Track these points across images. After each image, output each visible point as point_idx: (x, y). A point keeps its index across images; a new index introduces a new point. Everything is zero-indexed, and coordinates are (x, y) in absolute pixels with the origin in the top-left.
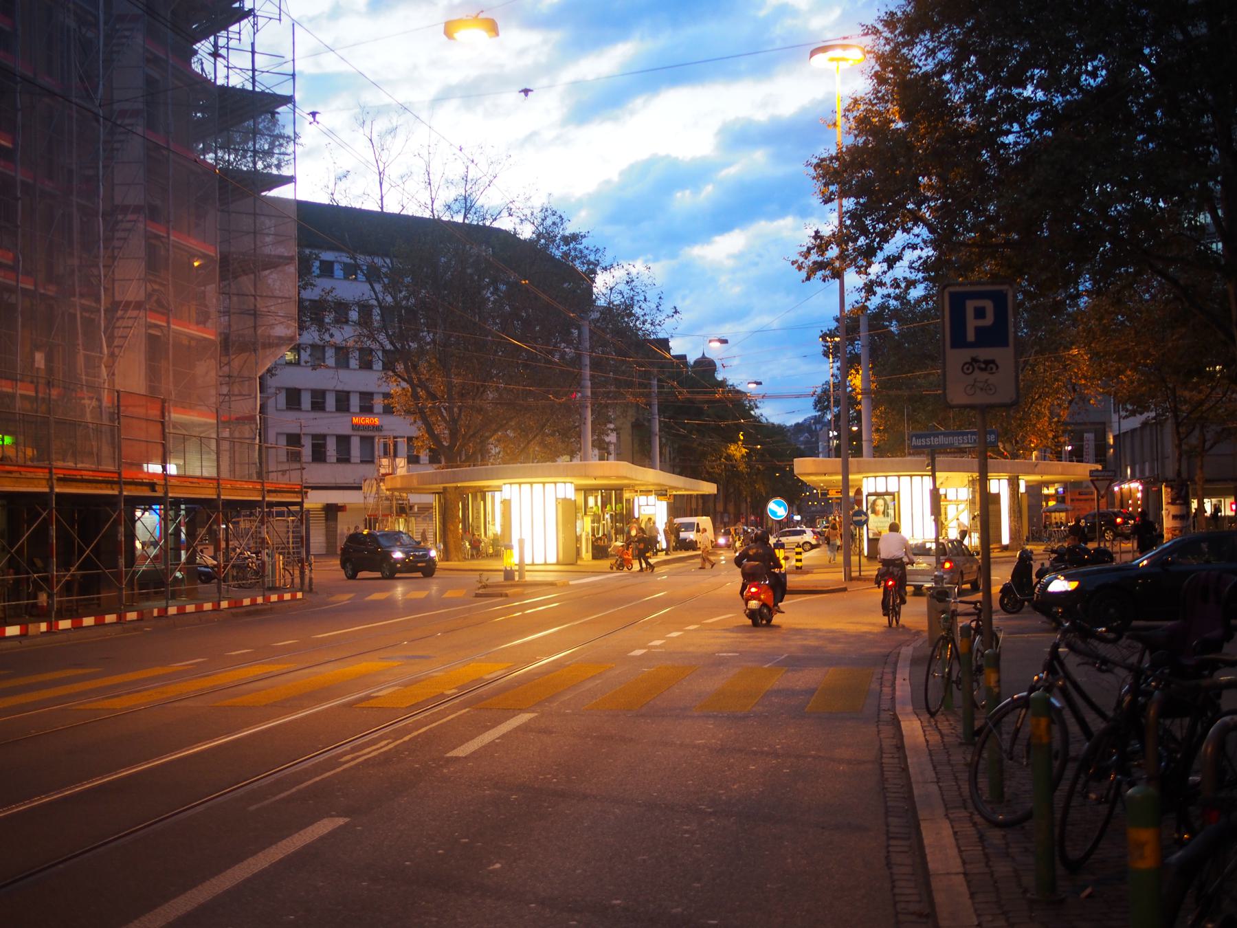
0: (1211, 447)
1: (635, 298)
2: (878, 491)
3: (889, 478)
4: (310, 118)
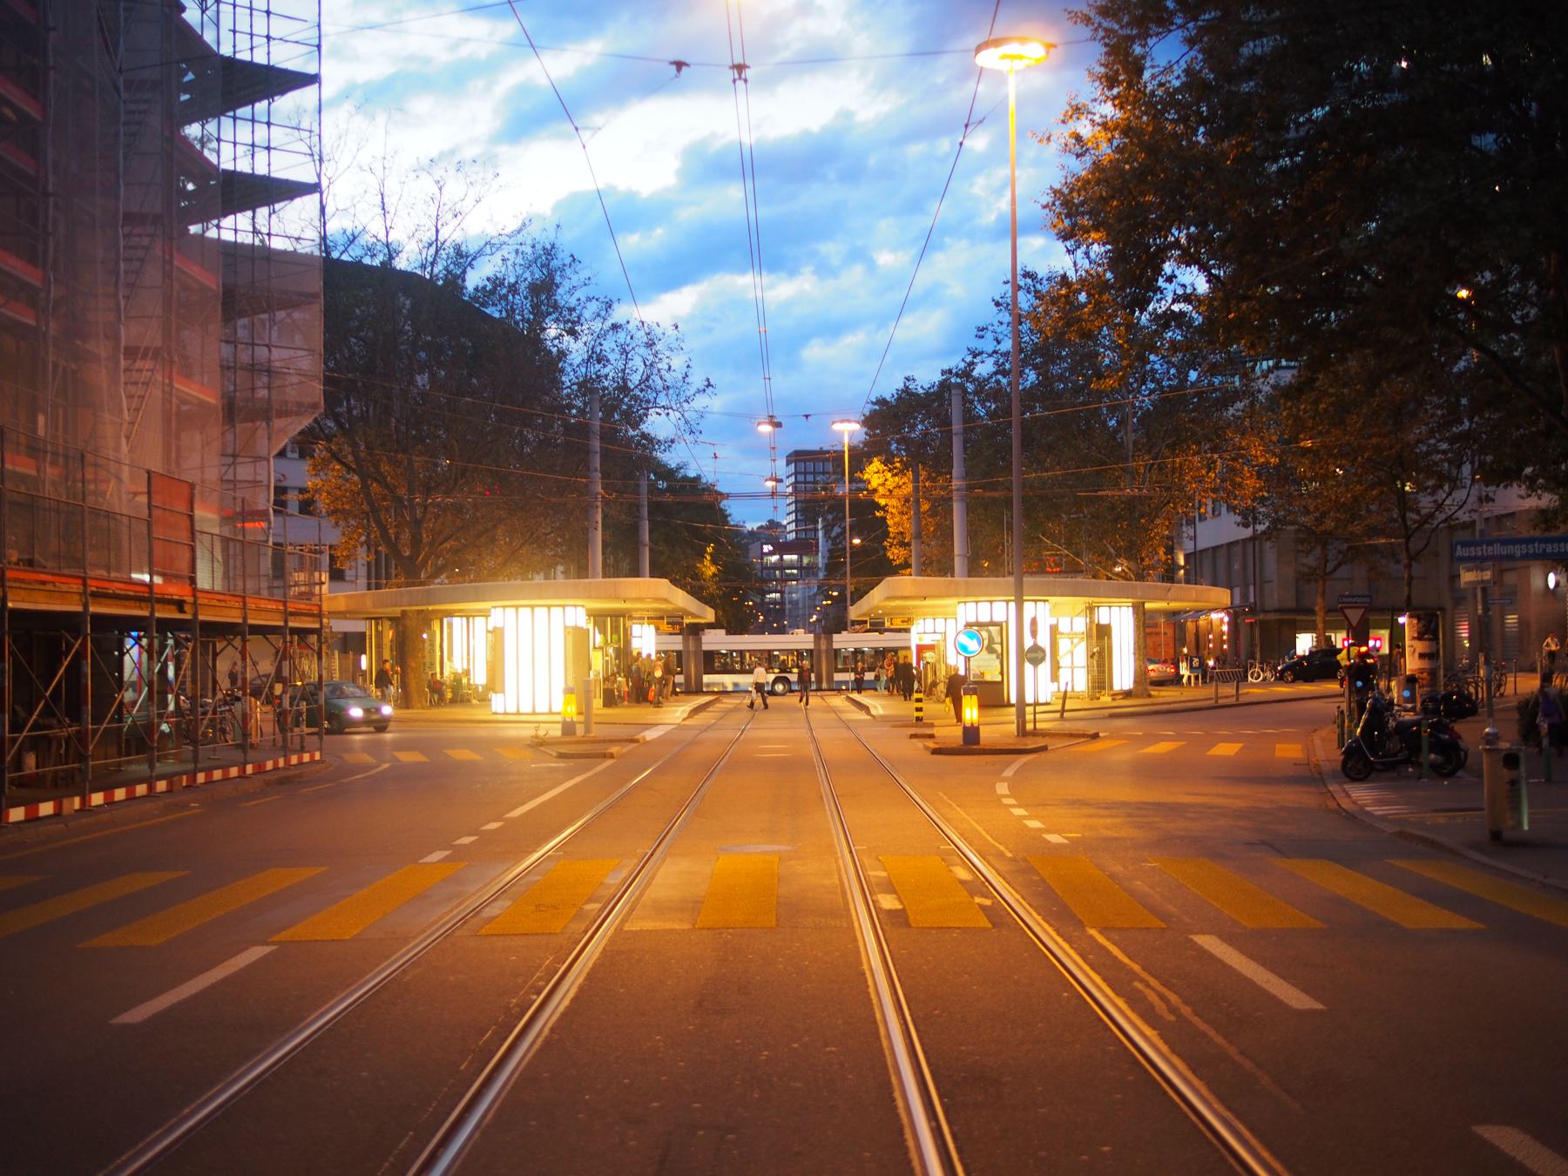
0: (1335, 569)
3: (994, 604)
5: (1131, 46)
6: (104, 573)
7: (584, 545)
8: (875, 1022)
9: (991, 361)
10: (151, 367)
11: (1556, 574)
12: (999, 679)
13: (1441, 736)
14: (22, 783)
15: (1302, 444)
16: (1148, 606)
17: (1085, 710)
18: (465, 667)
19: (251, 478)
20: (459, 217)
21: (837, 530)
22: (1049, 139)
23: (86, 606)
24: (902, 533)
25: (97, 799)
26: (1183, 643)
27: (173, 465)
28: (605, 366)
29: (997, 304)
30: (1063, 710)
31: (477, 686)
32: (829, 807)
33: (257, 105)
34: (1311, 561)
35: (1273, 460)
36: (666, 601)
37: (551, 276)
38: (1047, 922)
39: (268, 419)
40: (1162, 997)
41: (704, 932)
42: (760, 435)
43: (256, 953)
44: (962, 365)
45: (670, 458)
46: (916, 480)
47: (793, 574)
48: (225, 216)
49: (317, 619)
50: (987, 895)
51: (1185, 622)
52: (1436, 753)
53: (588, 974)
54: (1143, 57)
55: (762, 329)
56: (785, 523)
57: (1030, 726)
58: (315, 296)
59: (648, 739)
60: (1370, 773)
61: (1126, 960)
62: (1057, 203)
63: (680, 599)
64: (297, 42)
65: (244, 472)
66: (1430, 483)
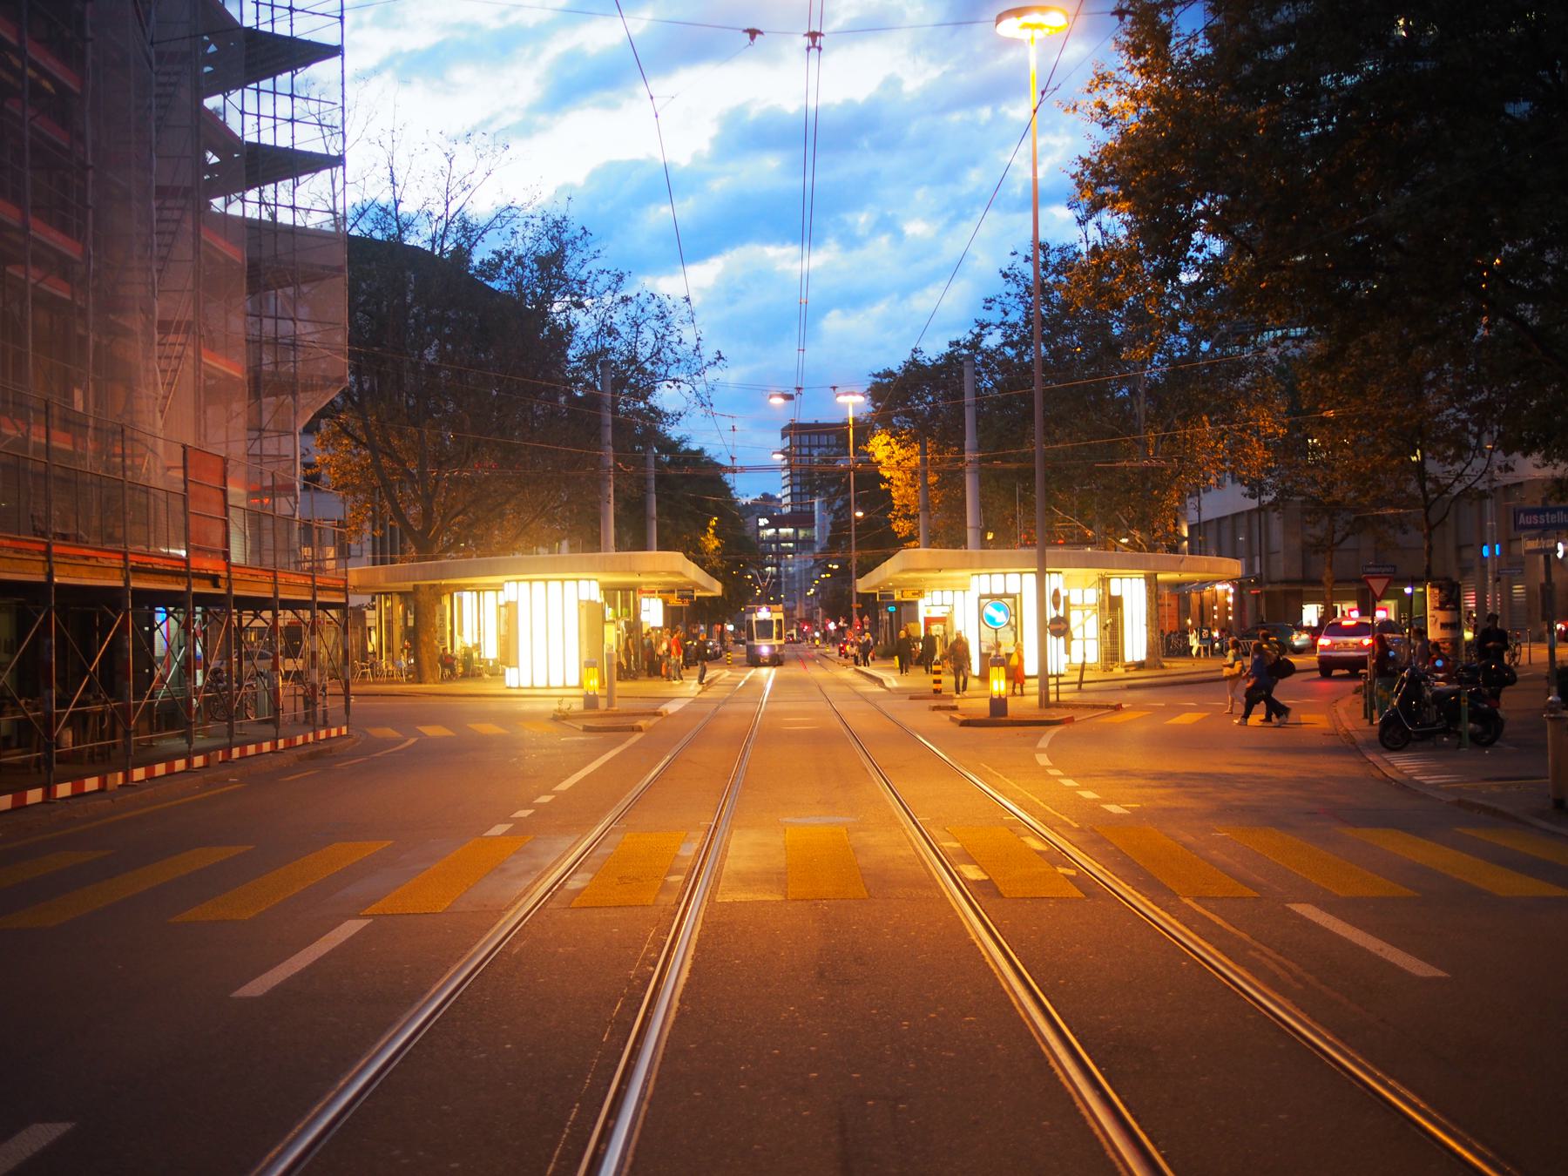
0: (1343, 540)
1: (667, 338)
2: (994, 592)
3: (1008, 576)
4: (807, 41)
5: (1157, 15)
6: (144, 548)
7: (596, 521)
8: (1003, 991)
9: (998, 332)
10: (183, 341)
11: (1563, 544)
13: (1480, 705)
14: (65, 759)
15: (1324, 414)
16: (1160, 577)
17: (1100, 681)
18: (476, 641)
19: (276, 453)
20: (470, 191)
21: (838, 503)
22: (1075, 108)
23: (127, 581)
24: (907, 506)
25: (139, 774)
26: (1187, 615)
27: (202, 438)
28: (615, 339)
29: (1005, 275)
30: (1081, 682)
31: (488, 661)
32: (876, 777)
33: (279, 78)
34: (1318, 531)
35: (1281, 431)
36: (681, 574)
37: (561, 250)
38: (1139, 892)
39: (294, 394)
40: (1281, 966)
41: (799, 903)
42: (773, 408)
43: (351, 927)
44: (970, 337)
45: (674, 432)
46: (923, 452)
47: (789, 548)
48: (249, 188)
49: (343, 594)
50: (1068, 866)
51: (1189, 594)
52: (1475, 723)
53: (696, 946)
54: (1170, 25)
55: (803, 301)
56: (779, 496)
57: (1053, 698)
58: (340, 269)
59: (670, 712)
60: (1406, 744)
61: (1232, 929)
62: (1087, 173)
63: (694, 573)
64: (323, 14)
65: (270, 446)
66: (1451, 452)
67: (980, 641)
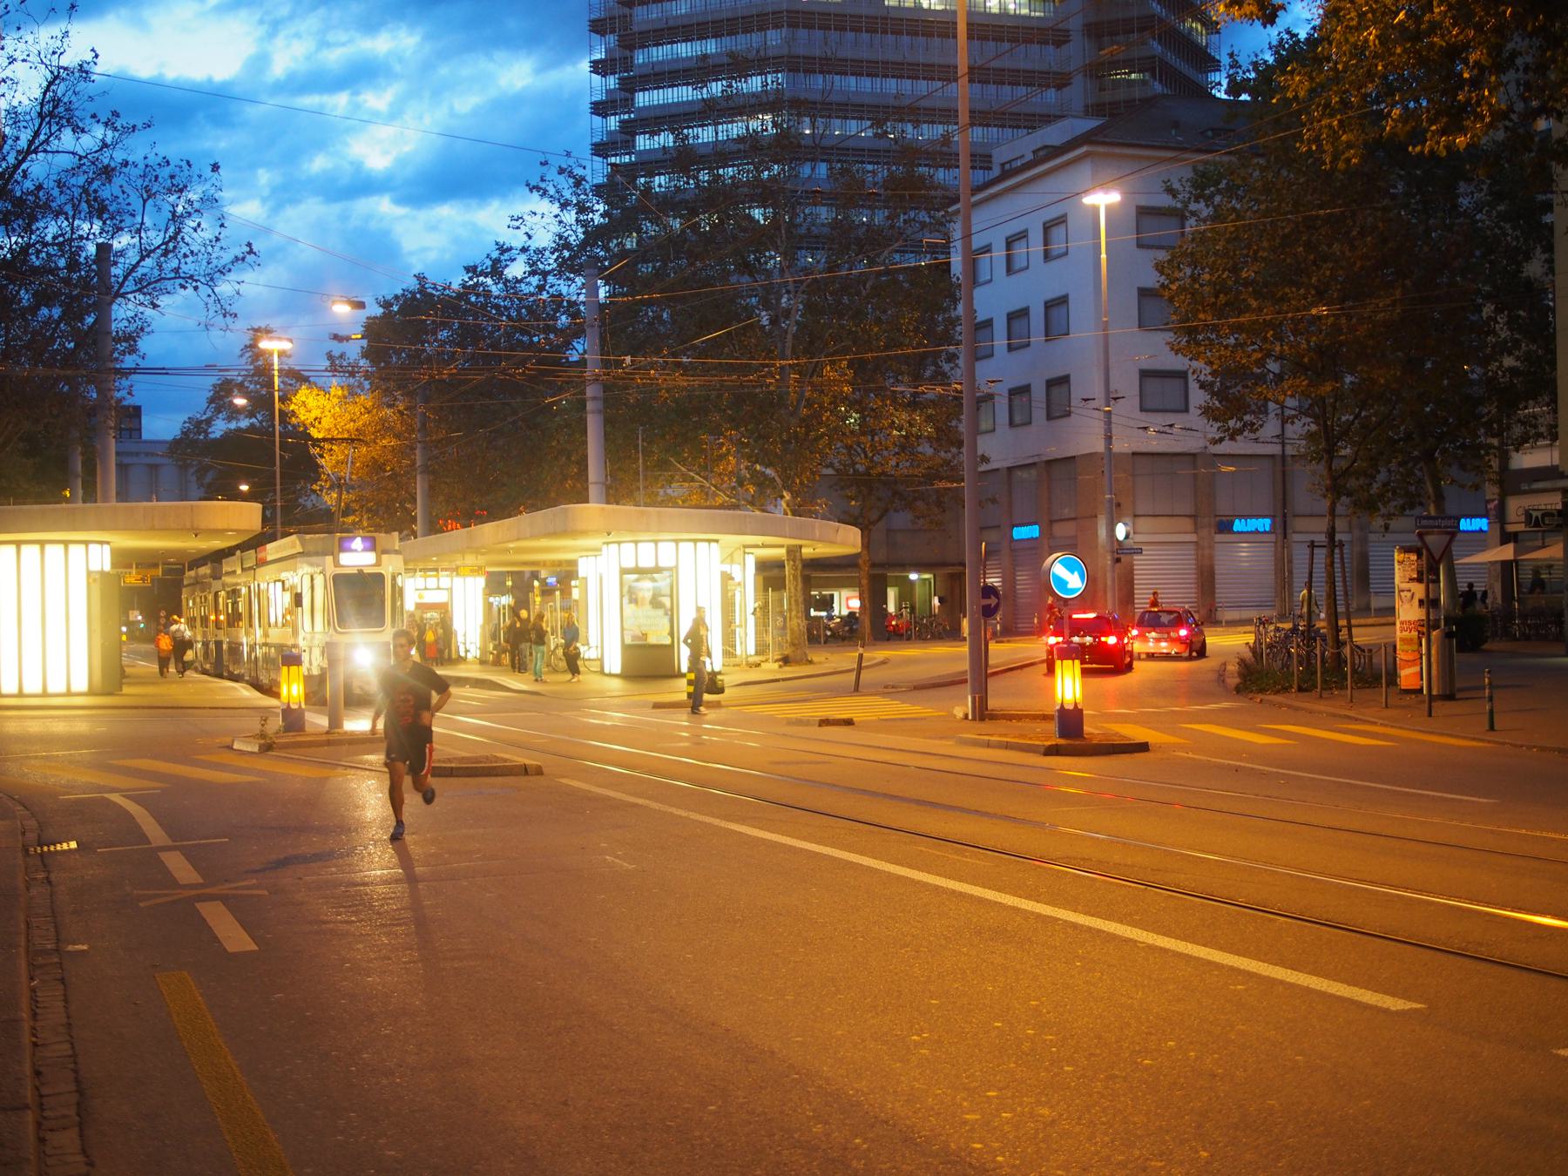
3: (660, 544)
9: (522, 258)
12: (668, 641)
67: (622, 629)
